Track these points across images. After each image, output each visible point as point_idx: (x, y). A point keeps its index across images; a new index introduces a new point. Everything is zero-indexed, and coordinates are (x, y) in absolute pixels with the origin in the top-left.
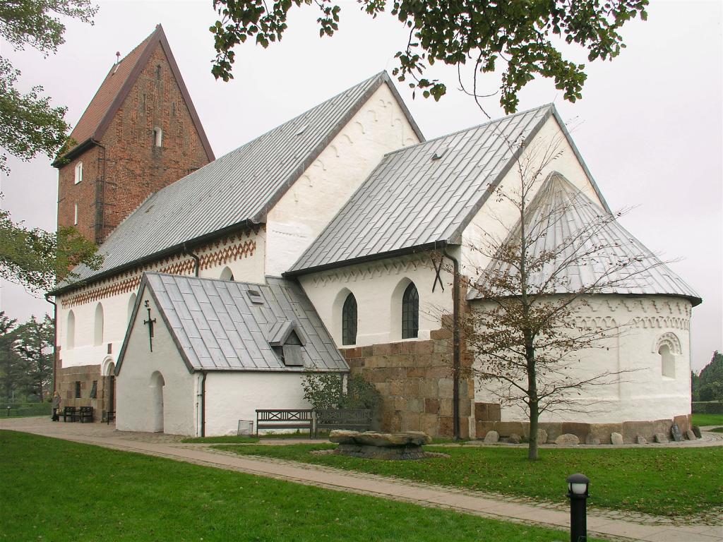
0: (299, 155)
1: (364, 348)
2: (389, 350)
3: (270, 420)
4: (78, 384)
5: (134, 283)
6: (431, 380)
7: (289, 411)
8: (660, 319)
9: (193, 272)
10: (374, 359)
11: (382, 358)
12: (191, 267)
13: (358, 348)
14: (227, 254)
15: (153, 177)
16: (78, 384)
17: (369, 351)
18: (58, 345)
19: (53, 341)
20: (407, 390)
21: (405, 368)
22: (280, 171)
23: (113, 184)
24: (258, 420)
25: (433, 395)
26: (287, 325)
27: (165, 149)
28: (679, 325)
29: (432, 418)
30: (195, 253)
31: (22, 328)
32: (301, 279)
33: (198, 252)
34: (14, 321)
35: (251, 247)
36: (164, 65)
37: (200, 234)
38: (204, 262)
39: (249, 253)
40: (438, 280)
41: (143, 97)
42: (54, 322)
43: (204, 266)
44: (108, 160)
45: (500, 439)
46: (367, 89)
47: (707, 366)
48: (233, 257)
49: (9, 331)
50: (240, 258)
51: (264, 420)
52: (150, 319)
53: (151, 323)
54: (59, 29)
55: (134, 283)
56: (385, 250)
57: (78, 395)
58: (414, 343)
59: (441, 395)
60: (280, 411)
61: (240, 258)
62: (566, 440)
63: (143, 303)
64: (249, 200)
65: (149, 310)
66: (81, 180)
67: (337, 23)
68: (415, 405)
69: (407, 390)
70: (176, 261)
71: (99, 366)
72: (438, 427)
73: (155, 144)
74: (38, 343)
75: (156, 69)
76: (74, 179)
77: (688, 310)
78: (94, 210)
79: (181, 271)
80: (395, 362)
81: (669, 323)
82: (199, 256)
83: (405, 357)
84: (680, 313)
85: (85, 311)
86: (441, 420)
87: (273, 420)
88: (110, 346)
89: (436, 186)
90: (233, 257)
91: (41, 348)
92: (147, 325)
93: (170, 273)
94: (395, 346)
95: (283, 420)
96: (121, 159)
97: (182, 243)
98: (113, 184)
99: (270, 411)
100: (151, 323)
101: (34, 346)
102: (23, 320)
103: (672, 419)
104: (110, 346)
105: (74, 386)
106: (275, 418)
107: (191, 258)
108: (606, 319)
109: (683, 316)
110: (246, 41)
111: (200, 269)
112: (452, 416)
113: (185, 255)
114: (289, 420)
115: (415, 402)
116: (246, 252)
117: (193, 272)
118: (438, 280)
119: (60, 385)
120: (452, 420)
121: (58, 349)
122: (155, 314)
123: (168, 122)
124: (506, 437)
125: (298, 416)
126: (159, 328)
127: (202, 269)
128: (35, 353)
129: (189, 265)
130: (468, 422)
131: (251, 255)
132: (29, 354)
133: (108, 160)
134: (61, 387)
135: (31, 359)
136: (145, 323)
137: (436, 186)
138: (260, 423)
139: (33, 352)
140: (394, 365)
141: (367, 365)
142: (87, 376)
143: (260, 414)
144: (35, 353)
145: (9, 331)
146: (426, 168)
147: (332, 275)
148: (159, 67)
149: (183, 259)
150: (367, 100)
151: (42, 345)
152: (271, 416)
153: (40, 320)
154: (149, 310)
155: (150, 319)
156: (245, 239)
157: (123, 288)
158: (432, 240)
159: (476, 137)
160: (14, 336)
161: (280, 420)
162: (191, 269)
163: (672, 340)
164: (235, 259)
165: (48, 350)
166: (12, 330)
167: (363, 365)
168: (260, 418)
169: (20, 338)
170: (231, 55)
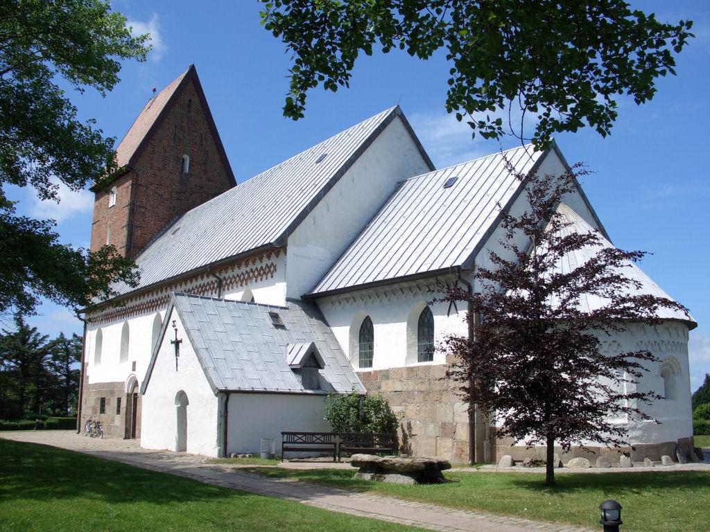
0: (318, 181)
1: (381, 371)
2: (405, 375)
3: (295, 442)
4: (103, 401)
5: (159, 302)
6: (447, 404)
7: (313, 434)
8: (660, 343)
9: (216, 292)
10: (390, 382)
11: (399, 382)
12: (214, 287)
13: (375, 372)
14: (249, 276)
15: (179, 201)
16: (103, 401)
17: (386, 374)
18: (86, 361)
19: (80, 357)
20: (423, 414)
21: (421, 391)
22: (300, 196)
23: (143, 207)
24: (284, 443)
25: (449, 419)
26: (306, 347)
27: (191, 175)
28: (678, 349)
29: (448, 442)
30: (217, 275)
31: (54, 343)
32: (326, 308)
33: (220, 273)
34: (47, 336)
35: (272, 269)
36: (195, 100)
37: (224, 256)
38: (226, 284)
39: (269, 275)
40: (453, 305)
41: (174, 128)
42: (83, 340)
43: (226, 287)
44: (141, 185)
45: (513, 463)
46: (381, 122)
47: (701, 388)
48: (254, 279)
49: (41, 346)
50: (261, 280)
51: (289, 443)
52: (176, 339)
53: (177, 343)
54: (115, 68)
55: (159, 302)
56: (401, 274)
57: (103, 411)
58: (429, 367)
59: (457, 419)
60: (305, 434)
61: (261, 280)
62: (577, 464)
63: (171, 323)
64: (271, 224)
65: (176, 330)
66: (114, 204)
67: (615, 110)
68: (432, 429)
69: (423, 414)
70: (200, 282)
71: (124, 382)
72: (454, 451)
73: (182, 171)
74: (65, 359)
75: (187, 103)
76: (108, 203)
77: (686, 332)
78: (125, 232)
79: (204, 292)
80: (411, 385)
81: (663, 348)
82: (222, 277)
83: (420, 380)
84: (670, 336)
85: (112, 331)
86: (457, 444)
87: (298, 443)
88: (134, 364)
89: (449, 212)
90: (254, 279)
91: (69, 363)
92: (174, 345)
93: (194, 293)
94: (411, 370)
95: (308, 443)
96: (151, 184)
97: (206, 265)
98: (143, 207)
99: (295, 434)
100: (177, 343)
101: (62, 361)
102: (54, 337)
103: (677, 441)
104: (134, 364)
105: (99, 401)
106: (300, 441)
107: (214, 279)
108: (612, 343)
109: (681, 340)
110: (317, 86)
111: (222, 290)
112: (468, 441)
113: (208, 276)
114: (314, 443)
115: (431, 427)
116: (262, 276)
117: (216, 292)
118: (453, 305)
119: (86, 401)
120: (468, 444)
121: (85, 366)
122: (182, 335)
123: (196, 150)
124: (520, 461)
125: (322, 439)
126: (185, 347)
127: (224, 290)
128: (62, 368)
129: (212, 286)
130: (483, 448)
131: (272, 277)
132: (57, 369)
133: (141, 185)
134: (88, 403)
135: (59, 374)
136: (172, 343)
137: (449, 212)
138: (285, 445)
139: (62, 368)
140: (411, 388)
141: (383, 389)
142: (112, 393)
143: (285, 436)
144: (62, 368)
145: (41, 346)
146: (438, 195)
147: (349, 298)
148: (190, 101)
149: (206, 280)
150: (381, 132)
151: (70, 361)
152: (296, 438)
153: (69, 337)
154: (176, 330)
155: (176, 339)
156: (266, 262)
157: (148, 307)
158: (447, 265)
159: (484, 167)
160: (45, 352)
161: (304, 442)
162: (214, 291)
163: (674, 366)
164: (256, 281)
165: (75, 366)
166: (43, 345)
167: (379, 388)
168: (285, 440)
169: (50, 353)
170: (303, 97)
